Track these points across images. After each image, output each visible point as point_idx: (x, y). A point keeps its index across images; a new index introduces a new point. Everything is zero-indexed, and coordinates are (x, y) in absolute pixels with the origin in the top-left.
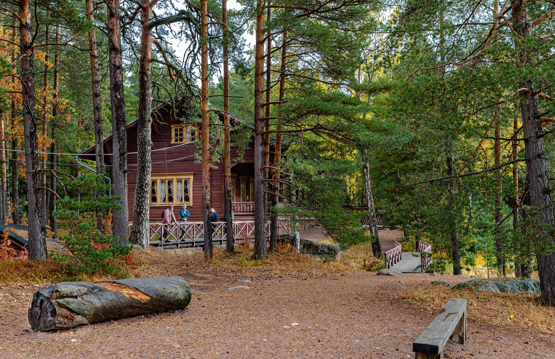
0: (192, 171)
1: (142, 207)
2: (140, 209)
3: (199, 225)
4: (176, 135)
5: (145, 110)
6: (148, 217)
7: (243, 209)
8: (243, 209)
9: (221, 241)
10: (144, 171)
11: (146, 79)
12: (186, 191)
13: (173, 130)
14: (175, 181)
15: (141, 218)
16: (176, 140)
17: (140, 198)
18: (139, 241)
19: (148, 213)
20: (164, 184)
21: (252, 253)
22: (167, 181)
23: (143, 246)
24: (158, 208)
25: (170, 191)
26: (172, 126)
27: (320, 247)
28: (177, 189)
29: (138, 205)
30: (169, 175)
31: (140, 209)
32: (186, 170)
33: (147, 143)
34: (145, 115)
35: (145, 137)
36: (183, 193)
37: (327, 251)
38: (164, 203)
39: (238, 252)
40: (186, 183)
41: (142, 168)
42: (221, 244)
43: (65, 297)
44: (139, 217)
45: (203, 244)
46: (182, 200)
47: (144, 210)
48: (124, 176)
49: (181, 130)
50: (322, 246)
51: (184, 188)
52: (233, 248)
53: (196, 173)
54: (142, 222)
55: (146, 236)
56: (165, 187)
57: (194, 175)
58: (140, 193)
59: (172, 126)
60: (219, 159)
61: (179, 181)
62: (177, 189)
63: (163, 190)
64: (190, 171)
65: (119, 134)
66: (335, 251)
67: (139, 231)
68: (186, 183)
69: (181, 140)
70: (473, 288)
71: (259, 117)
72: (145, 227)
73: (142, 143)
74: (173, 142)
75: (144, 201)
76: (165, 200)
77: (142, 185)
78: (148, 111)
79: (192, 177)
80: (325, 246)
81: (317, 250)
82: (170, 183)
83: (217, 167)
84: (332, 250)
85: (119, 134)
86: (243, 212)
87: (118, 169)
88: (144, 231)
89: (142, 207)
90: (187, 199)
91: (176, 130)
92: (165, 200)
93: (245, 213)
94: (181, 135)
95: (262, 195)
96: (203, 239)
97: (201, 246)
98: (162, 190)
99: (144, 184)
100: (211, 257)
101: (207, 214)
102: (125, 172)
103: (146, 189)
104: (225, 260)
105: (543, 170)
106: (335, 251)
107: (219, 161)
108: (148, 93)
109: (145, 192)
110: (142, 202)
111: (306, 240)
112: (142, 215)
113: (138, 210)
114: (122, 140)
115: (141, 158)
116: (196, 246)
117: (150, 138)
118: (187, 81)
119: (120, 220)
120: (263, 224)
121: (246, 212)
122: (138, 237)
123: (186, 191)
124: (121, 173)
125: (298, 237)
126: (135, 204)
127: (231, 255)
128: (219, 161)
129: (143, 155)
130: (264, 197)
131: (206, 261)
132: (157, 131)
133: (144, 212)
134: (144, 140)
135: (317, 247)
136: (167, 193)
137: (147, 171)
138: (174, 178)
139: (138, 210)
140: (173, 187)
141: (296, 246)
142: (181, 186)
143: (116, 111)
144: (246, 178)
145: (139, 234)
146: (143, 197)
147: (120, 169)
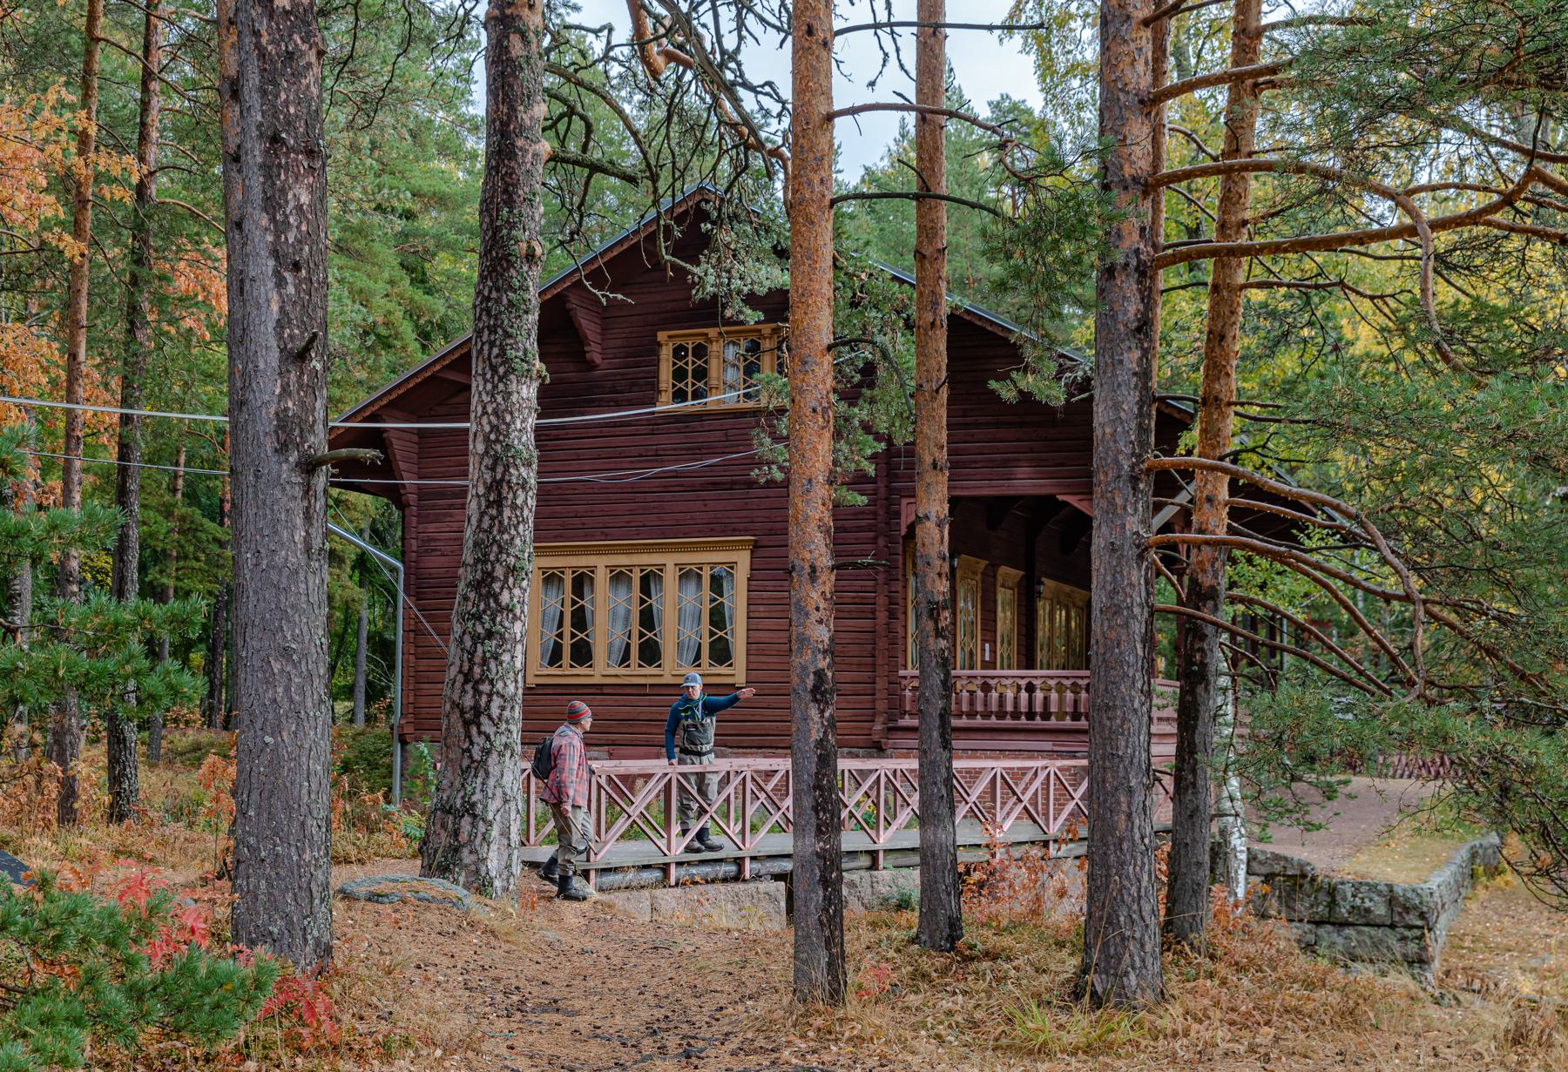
0: (745, 532)
1: (485, 687)
2: (477, 692)
3: (769, 774)
4: (679, 374)
5: (510, 203)
6: (516, 736)
7: (972, 703)
8: (972, 703)
9: (873, 854)
10: (499, 503)
11: (516, 48)
12: (718, 618)
13: (666, 353)
14: (670, 577)
15: (479, 741)
17: (477, 639)
18: (467, 858)
19: (517, 713)
20: (622, 590)
21: (1071, 964)
22: (636, 576)
23: (481, 885)
25: (647, 619)
26: (662, 336)
27: (1349, 891)
28: (681, 610)
29: (468, 676)
30: (650, 549)
31: (477, 692)
32: (717, 528)
33: (517, 364)
34: (512, 226)
35: (507, 335)
36: (706, 626)
37: (1380, 910)
38: (622, 671)
39: (987, 954)
40: (717, 584)
41: (489, 489)
42: (874, 866)
44: (468, 736)
45: (787, 866)
46: (698, 656)
47: (497, 702)
48: (307, 490)
49: (700, 351)
50: (1357, 887)
51: (707, 607)
52: (955, 926)
53: (765, 540)
54: (483, 763)
55: (505, 833)
56: (626, 601)
57: (756, 547)
58: (478, 617)
59: (662, 336)
60: (873, 458)
61: (688, 575)
63: (621, 612)
64: (734, 532)
65: (280, 228)
66: (1422, 916)
67: (469, 809)
68: (717, 584)
71: (1128, 171)
72: (499, 784)
73: (494, 369)
75: (496, 657)
76: (626, 658)
77: (489, 577)
78: (526, 210)
79: (743, 559)
80: (1373, 888)
81: (1333, 904)
82: (649, 581)
83: (862, 500)
84: (1407, 910)
85: (280, 228)
86: (1001, 715)
87: (270, 444)
88: (494, 805)
89: (485, 687)
90: (721, 653)
91: (678, 352)
92: (626, 658)
93: (979, 721)
94: (701, 374)
95: (1138, 628)
96: (785, 842)
97: (777, 877)
98: (614, 612)
99: (499, 572)
100: (835, 996)
101: (816, 735)
102: (309, 467)
103: (505, 597)
104: (913, 1000)
106: (1422, 916)
107: (871, 469)
108: (524, 117)
109: (501, 609)
110: (485, 662)
111: (1277, 857)
112: (487, 727)
113: (468, 701)
114: (296, 267)
115: (487, 440)
116: (757, 877)
117: (532, 345)
118: (722, 65)
119: (275, 764)
120: (1138, 798)
121: (986, 715)
122: (463, 837)
123: (718, 618)
124: (286, 471)
125: (1238, 842)
126: (453, 671)
127: (944, 972)
128: (871, 469)
129: (494, 428)
130: (1149, 640)
131: (802, 1023)
132: (597, 359)
133: (495, 712)
134: (503, 353)
135: (1332, 891)
136: (636, 627)
137: (514, 507)
138: (670, 562)
139: (468, 701)
140: (661, 601)
141: (1229, 881)
142: (696, 598)
143: (264, 93)
144: (983, 563)
145: (466, 823)
146: (490, 634)
147: (282, 449)
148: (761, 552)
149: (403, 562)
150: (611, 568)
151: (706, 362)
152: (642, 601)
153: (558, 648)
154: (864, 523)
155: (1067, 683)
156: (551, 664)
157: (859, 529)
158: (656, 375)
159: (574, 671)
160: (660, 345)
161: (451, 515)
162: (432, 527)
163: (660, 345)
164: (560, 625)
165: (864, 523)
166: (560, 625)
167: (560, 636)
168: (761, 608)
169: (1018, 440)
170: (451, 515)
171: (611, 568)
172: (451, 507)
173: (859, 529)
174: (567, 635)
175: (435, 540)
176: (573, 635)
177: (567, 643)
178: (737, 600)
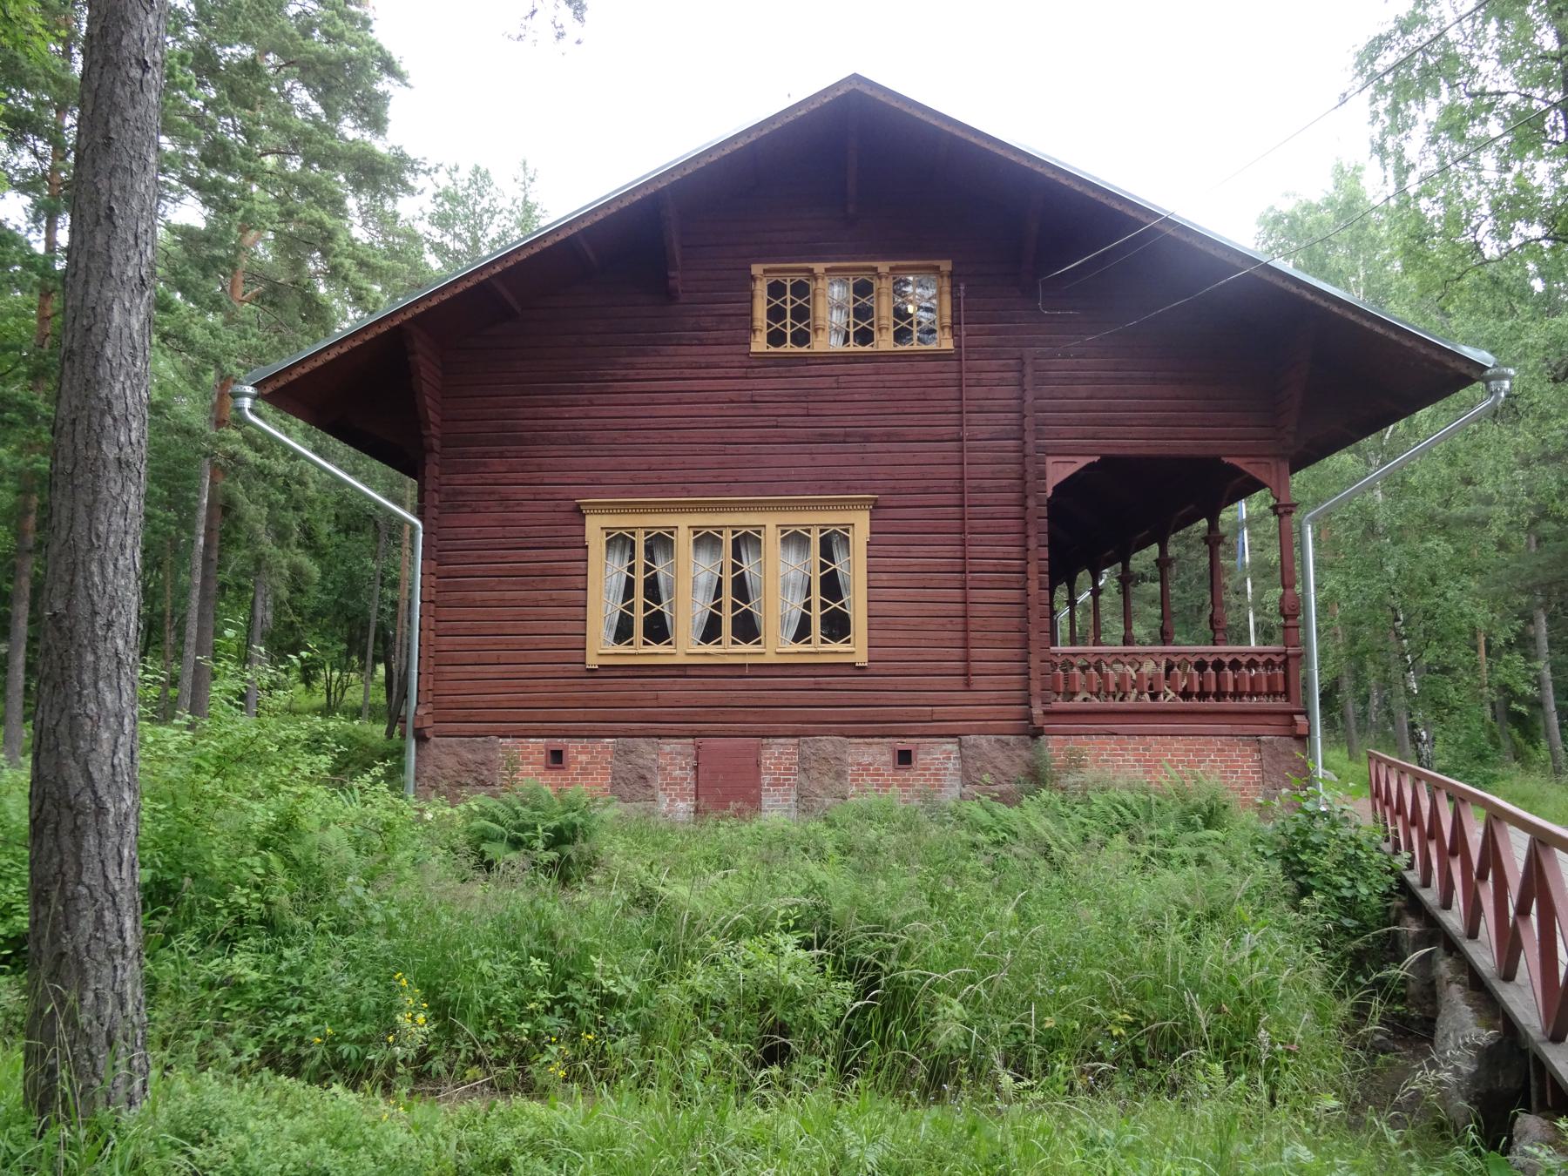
0: (863, 490)
4: (776, 314)
13: (761, 290)
16: (776, 338)
24: (681, 671)
26: (757, 269)
28: (782, 582)
43: (1357, 677)
49: (801, 289)
51: (817, 576)
53: (886, 500)
57: (876, 507)
59: (757, 269)
62: (782, 582)
64: (856, 490)
69: (801, 338)
70: (240, 213)
74: (759, 344)
79: (860, 524)
82: (660, 543)
91: (776, 290)
92: (803, 632)
94: (801, 314)
105: (344, 902)
123: (831, 586)
148: (882, 513)
149: (420, 514)
150: (783, 528)
151: (808, 301)
152: (823, 567)
153: (805, 622)
154: (1004, 482)
155: (1210, 660)
156: (796, 639)
157: (1000, 490)
158: (750, 313)
159: (649, 649)
160: (753, 279)
161: (485, 464)
162: (459, 479)
163: (753, 279)
164: (718, 593)
165: (1004, 482)
166: (718, 593)
167: (807, 606)
168: (884, 576)
169: (1178, 398)
170: (485, 464)
171: (783, 528)
172: (485, 455)
173: (1000, 490)
174: (816, 606)
175: (462, 493)
176: (824, 605)
177: (816, 614)
178: (854, 568)
